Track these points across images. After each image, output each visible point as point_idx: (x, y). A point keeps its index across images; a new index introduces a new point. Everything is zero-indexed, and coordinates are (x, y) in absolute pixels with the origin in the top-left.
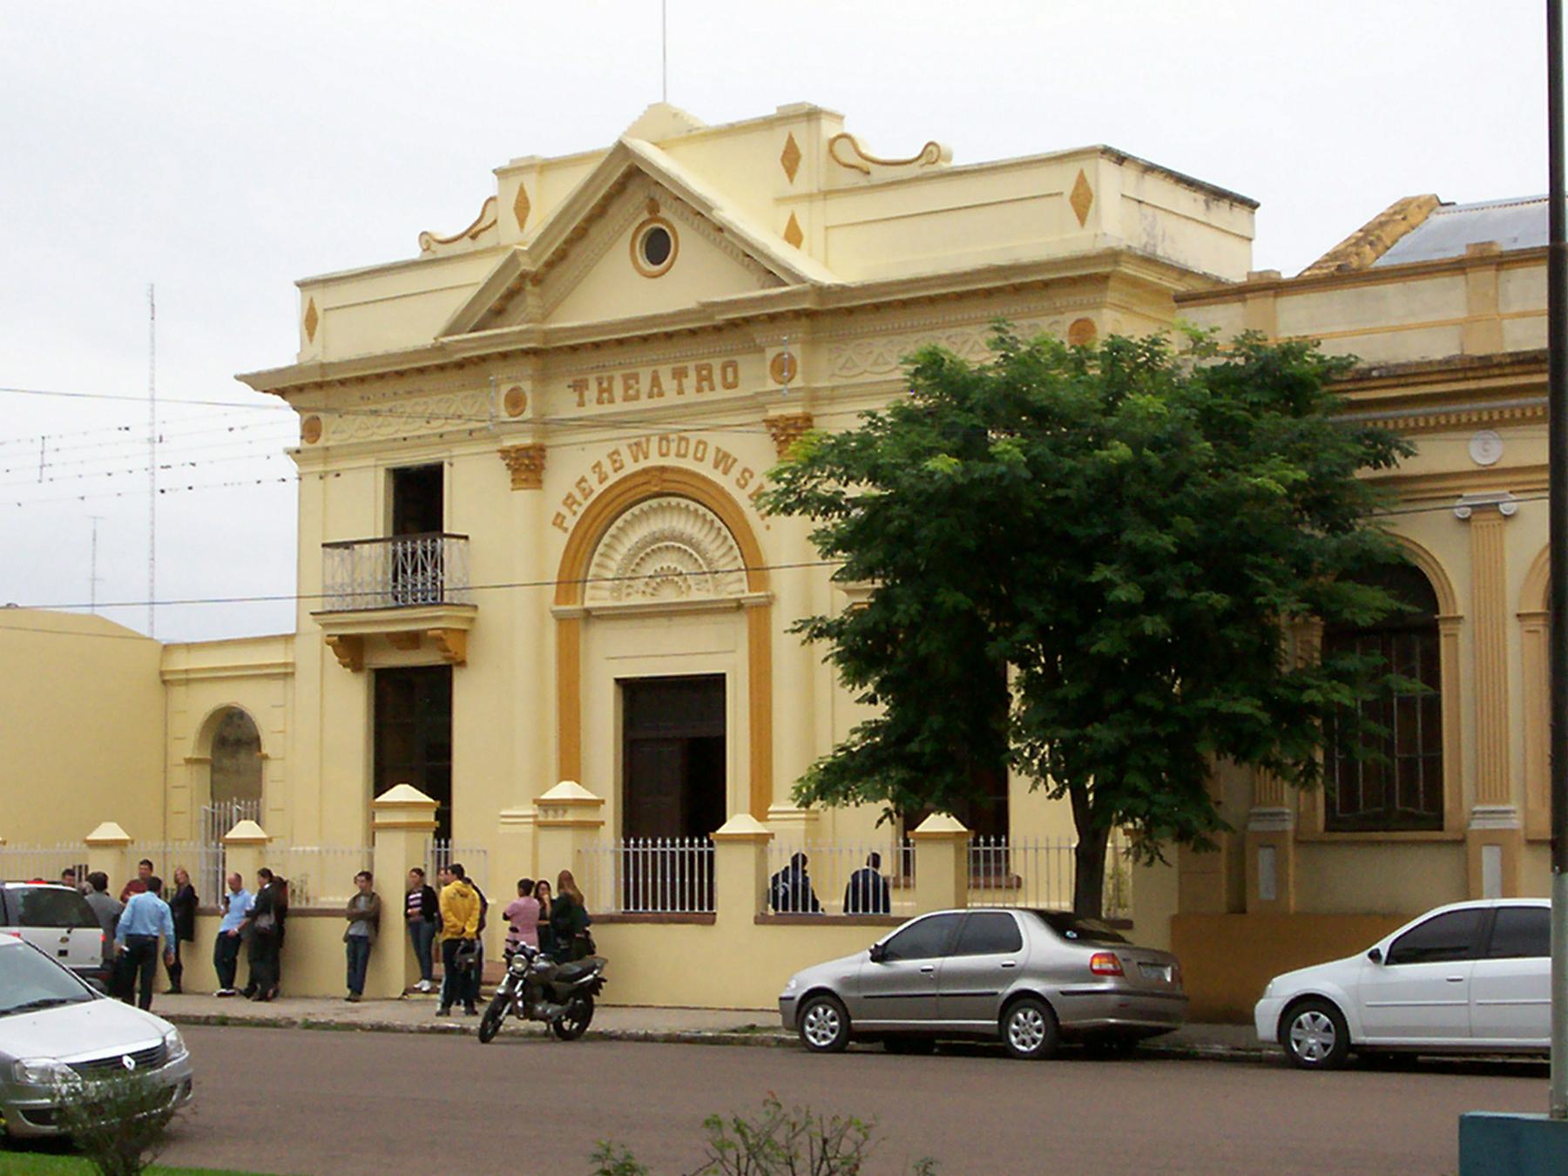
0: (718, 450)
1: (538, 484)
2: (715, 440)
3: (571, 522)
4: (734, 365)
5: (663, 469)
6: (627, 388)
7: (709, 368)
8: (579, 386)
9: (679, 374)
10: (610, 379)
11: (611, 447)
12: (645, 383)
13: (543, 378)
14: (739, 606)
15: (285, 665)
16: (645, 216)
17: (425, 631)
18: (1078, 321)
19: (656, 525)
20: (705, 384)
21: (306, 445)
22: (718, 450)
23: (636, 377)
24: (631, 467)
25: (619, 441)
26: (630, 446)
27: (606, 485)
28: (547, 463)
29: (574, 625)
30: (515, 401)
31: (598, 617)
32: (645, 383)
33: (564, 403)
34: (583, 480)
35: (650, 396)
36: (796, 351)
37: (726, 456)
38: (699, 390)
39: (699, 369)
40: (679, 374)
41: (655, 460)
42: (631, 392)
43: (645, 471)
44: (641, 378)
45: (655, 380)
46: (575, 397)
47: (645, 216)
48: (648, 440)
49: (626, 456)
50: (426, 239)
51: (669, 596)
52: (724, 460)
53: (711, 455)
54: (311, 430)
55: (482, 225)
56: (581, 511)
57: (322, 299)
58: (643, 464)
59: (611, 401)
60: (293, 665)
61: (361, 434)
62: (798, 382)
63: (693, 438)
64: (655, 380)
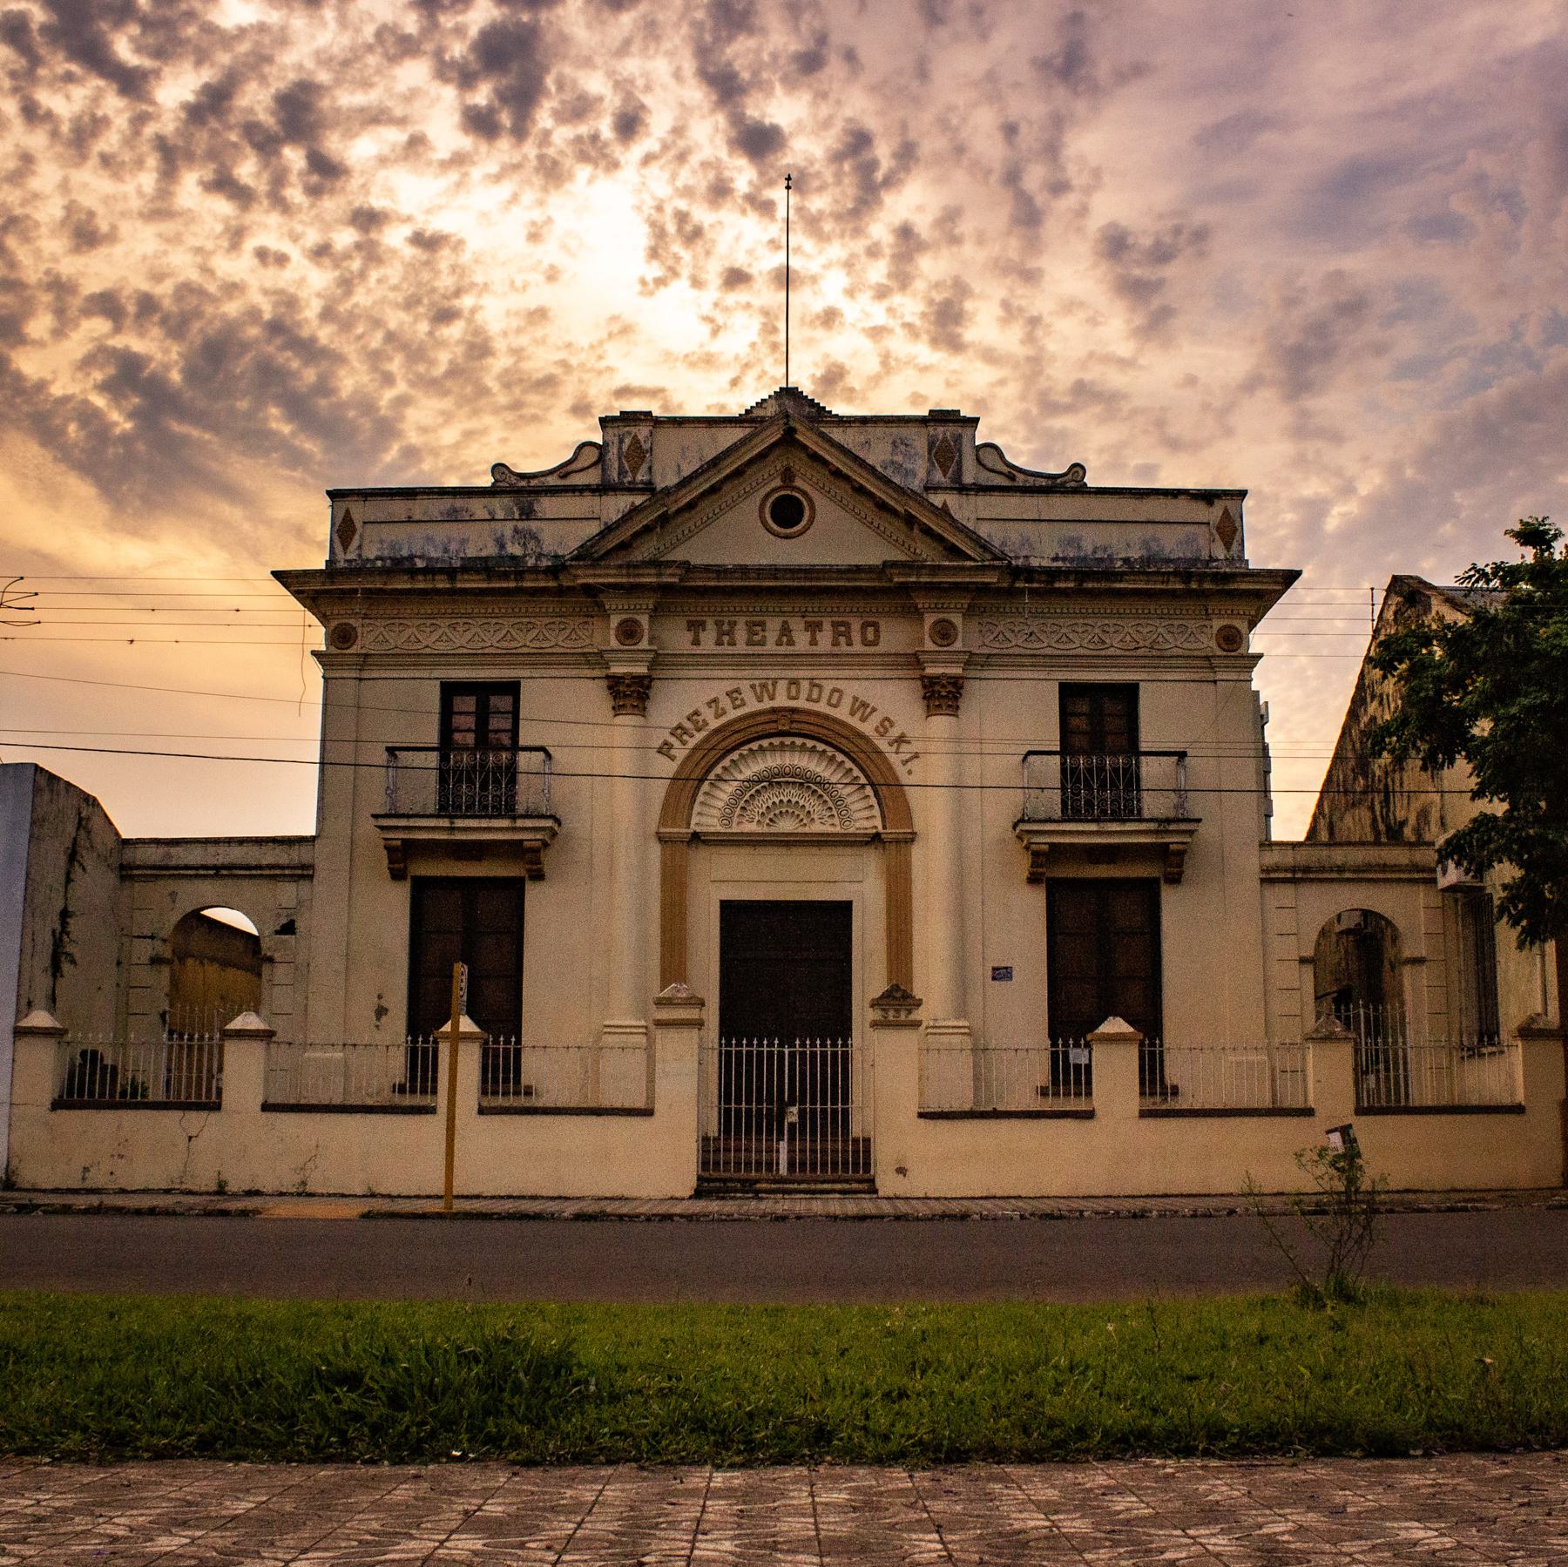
0: (856, 699)
1: (642, 710)
2: (852, 689)
3: (680, 753)
4: (875, 625)
5: (794, 710)
6: (752, 633)
7: (847, 625)
8: (696, 626)
9: (813, 627)
10: (733, 624)
11: (729, 686)
12: (772, 634)
13: (656, 613)
14: (875, 839)
15: (303, 867)
16: (777, 482)
17: (521, 841)
18: (1225, 627)
19: (772, 762)
20: (726, 639)
21: (334, 650)
22: (856, 699)
23: (762, 624)
24: (753, 706)
25: (744, 681)
26: (753, 687)
27: (723, 720)
28: (652, 693)
29: (682, 844)
30: (629, 632)
31: (704, 842)
32: (772, 634)
33: (677, 638)
34: (696, 713)
35: (779, 643)
36: (957, 619)
37: (864, 705)
38: (719, 643)
39: (835, 625)
40: (813, 627)
41: (781, 701)
42: (756, 638)
43: (774, 710)
44: (769, 625)
45: (786, 630)
46: (689, 636)
47: (777, 482)
48: (774, 685)
49: (748, 695)
50: (499, 469)
51: (786, 826)
52: (862, 707)
53: (847, 703)
54: (340, 637)
55: (573, 467)
56: (692, 743)
57: (359, 511)
58: (767, 704)
59: (732, 643)
60: (311, 867)
61: (569, 644)
62: (958, 646)
63: (828, 686)
64: (786, 630)
